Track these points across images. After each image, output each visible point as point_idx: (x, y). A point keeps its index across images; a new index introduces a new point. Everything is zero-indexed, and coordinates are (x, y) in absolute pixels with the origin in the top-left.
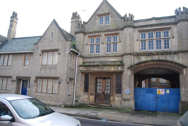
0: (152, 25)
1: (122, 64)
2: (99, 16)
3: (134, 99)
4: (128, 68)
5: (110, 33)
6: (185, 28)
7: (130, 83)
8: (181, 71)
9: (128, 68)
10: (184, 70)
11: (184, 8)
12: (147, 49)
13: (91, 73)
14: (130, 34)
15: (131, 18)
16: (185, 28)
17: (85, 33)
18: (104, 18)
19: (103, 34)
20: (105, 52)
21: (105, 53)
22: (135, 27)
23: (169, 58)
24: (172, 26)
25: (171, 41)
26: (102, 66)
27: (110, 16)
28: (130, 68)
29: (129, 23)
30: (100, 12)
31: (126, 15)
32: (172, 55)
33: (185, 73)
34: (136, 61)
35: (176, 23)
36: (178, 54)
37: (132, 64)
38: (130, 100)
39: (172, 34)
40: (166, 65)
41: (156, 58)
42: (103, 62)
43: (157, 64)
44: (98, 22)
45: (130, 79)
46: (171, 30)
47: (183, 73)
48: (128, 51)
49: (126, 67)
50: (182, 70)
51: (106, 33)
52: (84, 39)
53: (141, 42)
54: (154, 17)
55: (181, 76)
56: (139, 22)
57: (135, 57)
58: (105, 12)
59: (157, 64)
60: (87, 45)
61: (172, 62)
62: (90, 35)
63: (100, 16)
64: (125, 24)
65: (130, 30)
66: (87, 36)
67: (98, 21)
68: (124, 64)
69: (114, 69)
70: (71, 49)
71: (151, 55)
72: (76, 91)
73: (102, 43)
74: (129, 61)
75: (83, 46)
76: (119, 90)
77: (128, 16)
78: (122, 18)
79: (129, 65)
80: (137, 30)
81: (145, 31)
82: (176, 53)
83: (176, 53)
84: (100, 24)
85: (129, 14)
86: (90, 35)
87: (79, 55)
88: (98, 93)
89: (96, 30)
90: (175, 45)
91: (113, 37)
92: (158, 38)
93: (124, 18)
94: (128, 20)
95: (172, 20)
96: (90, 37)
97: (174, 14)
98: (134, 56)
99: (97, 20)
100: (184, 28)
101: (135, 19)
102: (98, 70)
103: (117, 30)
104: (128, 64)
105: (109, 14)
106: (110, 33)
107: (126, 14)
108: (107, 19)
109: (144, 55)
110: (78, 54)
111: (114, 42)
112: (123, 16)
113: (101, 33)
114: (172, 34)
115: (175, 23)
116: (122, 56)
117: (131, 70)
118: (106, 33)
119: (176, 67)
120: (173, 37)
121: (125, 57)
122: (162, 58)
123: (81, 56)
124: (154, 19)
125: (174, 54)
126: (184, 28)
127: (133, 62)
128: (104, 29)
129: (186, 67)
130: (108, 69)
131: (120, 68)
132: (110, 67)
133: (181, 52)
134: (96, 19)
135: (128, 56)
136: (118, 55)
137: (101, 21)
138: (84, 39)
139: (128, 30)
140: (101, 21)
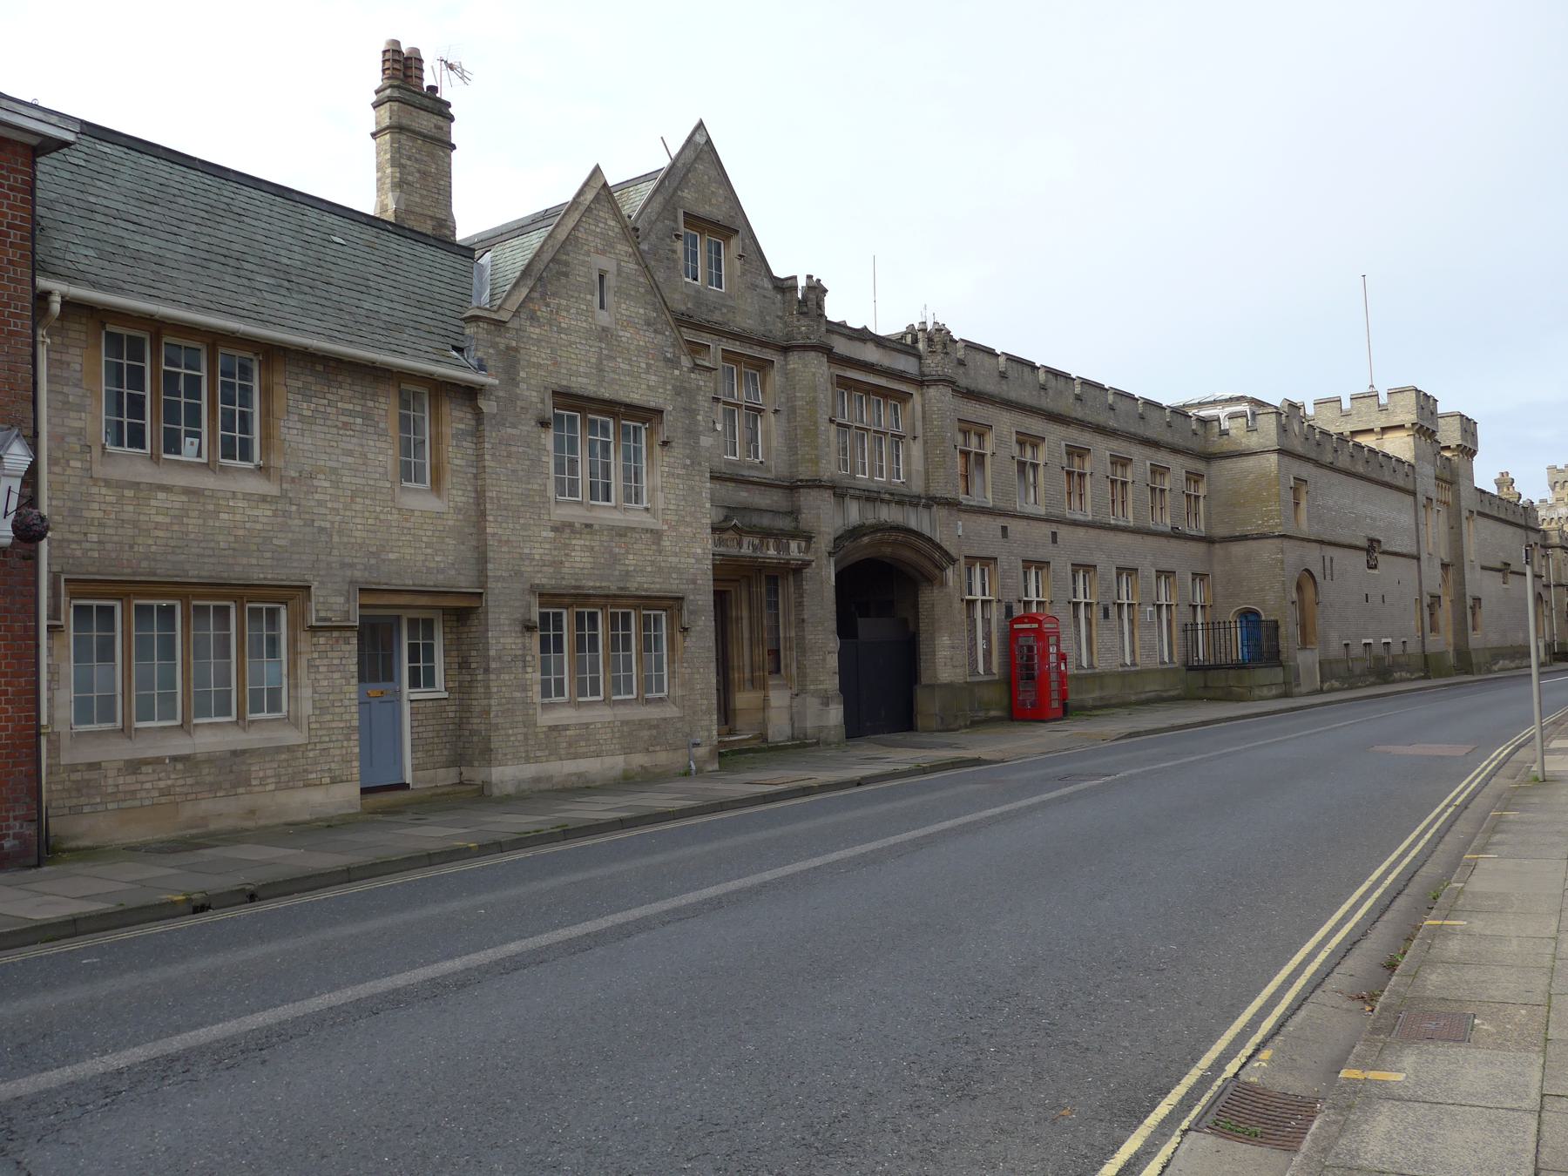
10: (950, 572)
23: (916, 520)
47: (943, 584)
50: (943, 569)
51: (736, 347)
69: (778, 549)
74: (827, 519)
83: (931, 502)
103: (763, 344)
112: (780, 271)
116: (793, 487)
118: (736, 347)
131: (794, 549)
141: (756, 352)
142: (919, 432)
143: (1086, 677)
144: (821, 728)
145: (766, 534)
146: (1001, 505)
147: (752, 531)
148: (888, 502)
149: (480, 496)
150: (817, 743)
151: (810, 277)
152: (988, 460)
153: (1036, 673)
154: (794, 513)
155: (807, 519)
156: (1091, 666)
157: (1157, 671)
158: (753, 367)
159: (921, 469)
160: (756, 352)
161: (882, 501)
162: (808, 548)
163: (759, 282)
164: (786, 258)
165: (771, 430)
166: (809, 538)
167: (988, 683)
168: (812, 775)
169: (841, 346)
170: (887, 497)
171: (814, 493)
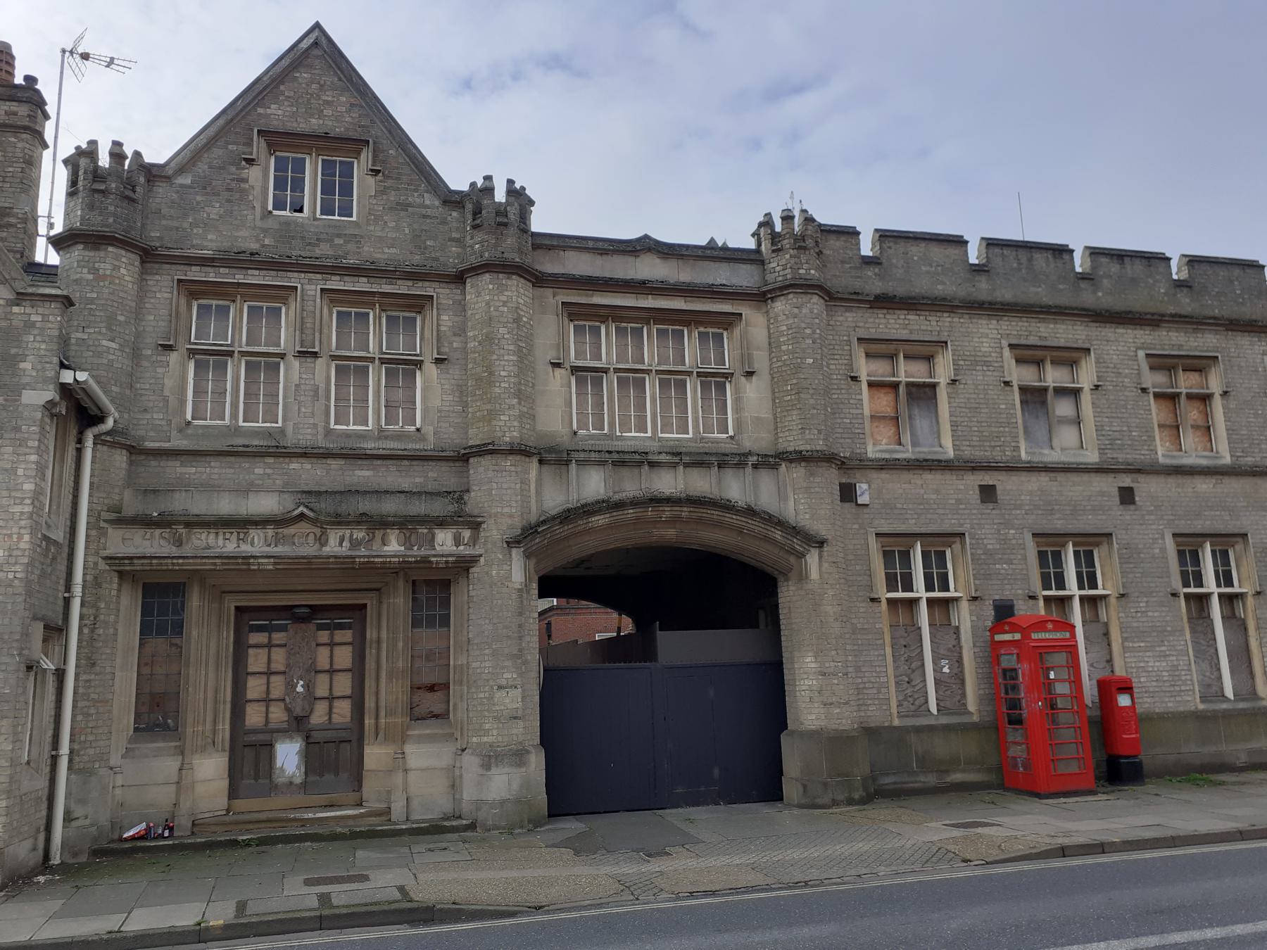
0: (641, 287)
1: (466, 520)
2: (269, 145)
3: (542, 743)
4: (512, 543)
5: (362, 285)
6: (814, 332)
7: (520, 638)
8: (792, 559)
9: (512, 543)
10: (812, 559)
11: (117, 153)
12: (234, 415)
13: (199, 576)
14: (517, 320)
15: (524, 216)
16: (814, 332)
17: (149, 256)
18: (312, 171)
19: (310, 287)
20: (328, 422)
21: (329, 432)
22: (539, 280)
23: (735, 488)
24: (745, 310)
25: (286, 370)
26: (314, 522)
27: (360, 167)
28: (527, 537)
29: (509, 246)
30: (277, 114)
31: (473, 185)
32: (749, 470)
33: (814, 574)
34: (555, 498)
35: (764, 293)
36: (775, 467)
37: (533, 518)
38: (528, 752)
39: (746, 358)
40: (719, 525)
41: (668, 483)
42: (319, 493)
43: (674, 521)
44: (265, 189)
45: (521, 614)
46: (737, 331)
47: (803, 577)
48: (508, 429)
49: (494, 532)
50: (801, 556)
51: (335, 283)
52: (142, 292)
53: (192, 365)
54: (646, 236)
55: (788, 595)
56: (564, 248)
57: (545, 468)
58: (309, 112)
59: (674, 521)
60: (168, 348)
61: (750, 512)
62: (195, 274)
63: (277, 139)
64: (479, 246)
65: (516, 291)
66: (163, 287)
67: (262, 178)
68: (476, 512)
69: (407, 543)
70: (67, 377)
71: (639, 464)
72: (72, 728)
73: (302, 354)
74: (509, 496)
75: (136, 355)
76: (431, 699)
77: (500, 196)
78: (453, 200)
79: (518, 523)
80: (555, 298)
81: (602, 312)
82: (771, 461)
83: (771, 461)
84: (279, 205)
85: (117, 144)
86: (195, 274)
87: (110, 423)
88: (255, 731)
89: (246, 240)
90: (758, 418)
91: (384, 320)
92: (671, 368)
93: (474, 203)
94: (505, 225)
95: (743, 277)
96: (574, 312)
97: (751, 244)
98: (541, 462)
99: (254, 173)
100: (808, 331)
101: (539, 223)
102: (280, 550)
103: (415, 276)
104: (511, 516)
105: (354, 145)
106: (362, 285)
107: (488, 178)
108: (337, 190)
109: (602, 463)
110: (100, 419)
111: (250, 349)
112: (458, 181)
113: (293, 279)
114: (746, 358)
115: (761, 297)
116: (463, 457)
117: (528, 556)
118: (335, 283)
119: (774, 542)
120: (750, 374)
121: (481, 469)
122: (700, 483)
123: (117, 440)
124: (645, 246)
125: (755, 466)
126: (808, 331)
127: (534, 508)
128: (318, 252)
129: (821, 543)
130: (355, 544)
131: (444, 541)
132: (379, 534)
133: (791, 461)
134: (250, 161)
135: (508, 463)
136: (430, 444)
137: (290, 183)
138: (142, 292)
139: (502, 289)
140: (290, 183)
141: (403, 288)
142: (761, 361)
143: (1228, 716)
144: (479, 803)
145: (405, 524)
146: (968, 453)
147: (339, 521)
148: (674, 466)
149: (520, 451)
150: (472, 826)
151: (511, 182)
152: (942, 394)
153: (1025, 714)
154: (459, 496)
155: (477, 500)
156: (1247, 691)
157: (1197, 716)
158: (410, 308)
159: (766, 414)
160: (403, 288)
161: (653, 465)
162: (474, 540)
163: (414, 199)
164: (459, 158)
165: (429, 386)
166: (475, 526)
167: (947, 728)
168: (1070, 826)
169: (550, 265)
170: (664, 458)
171: (486, 461)
